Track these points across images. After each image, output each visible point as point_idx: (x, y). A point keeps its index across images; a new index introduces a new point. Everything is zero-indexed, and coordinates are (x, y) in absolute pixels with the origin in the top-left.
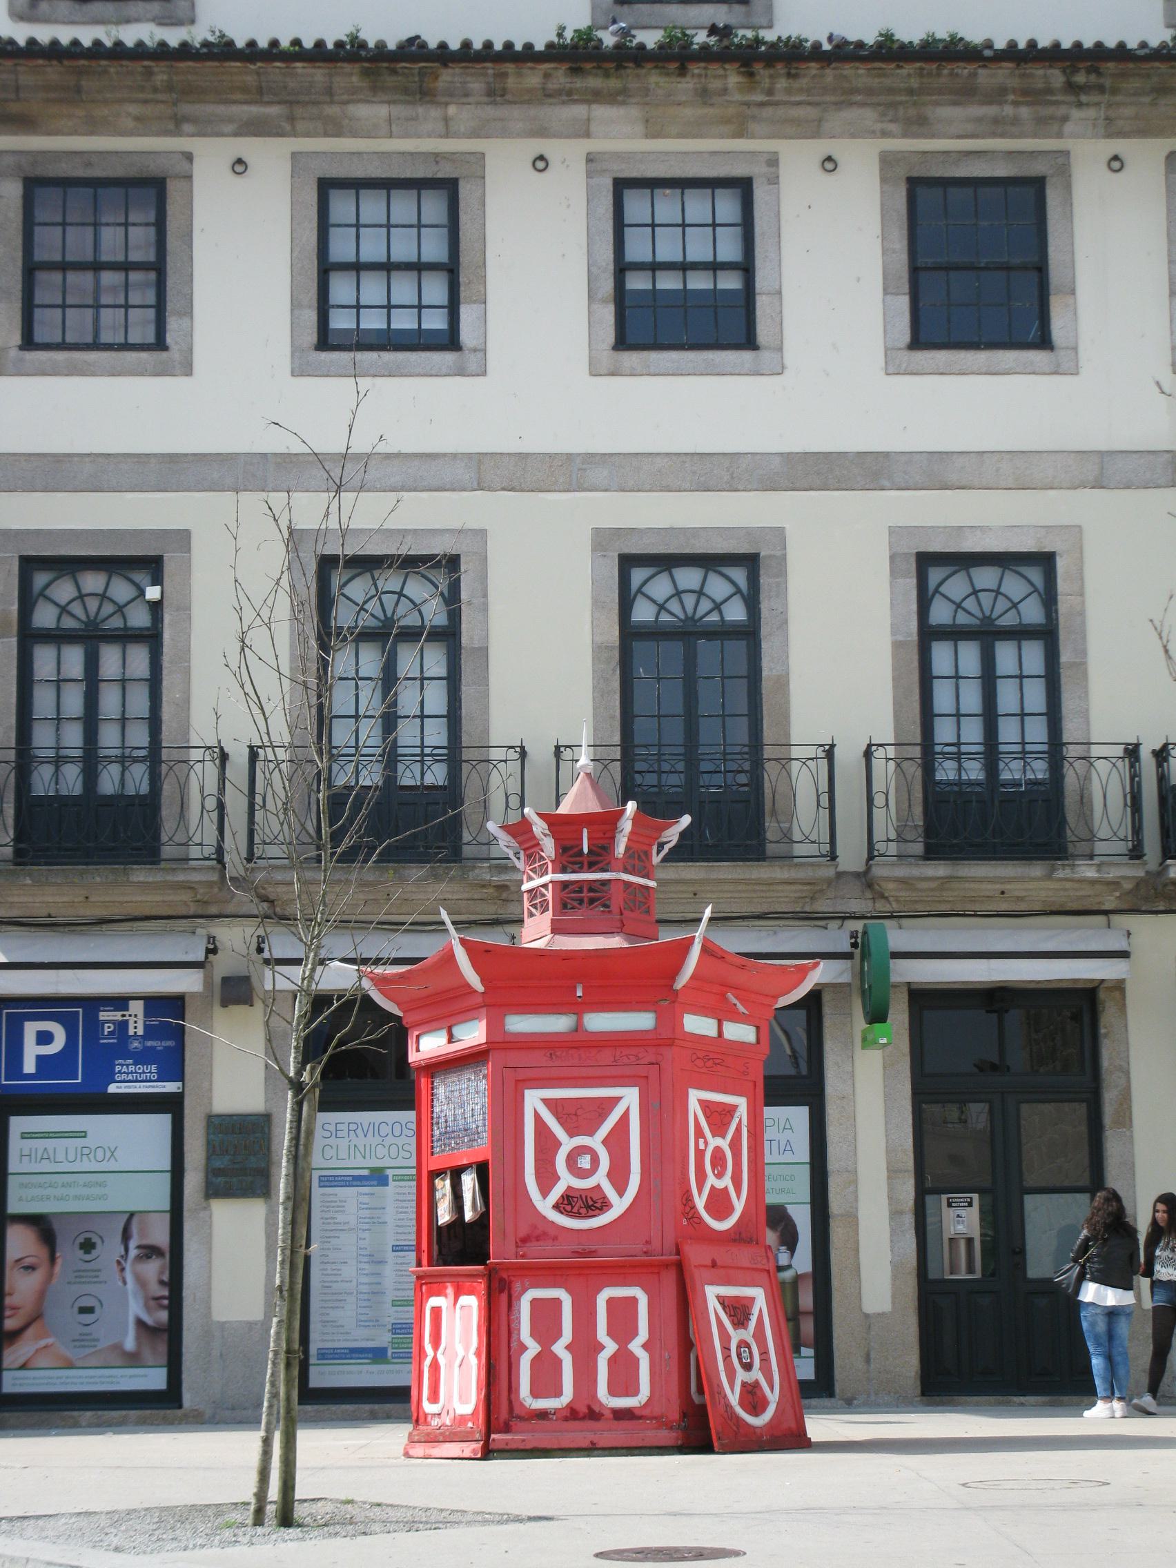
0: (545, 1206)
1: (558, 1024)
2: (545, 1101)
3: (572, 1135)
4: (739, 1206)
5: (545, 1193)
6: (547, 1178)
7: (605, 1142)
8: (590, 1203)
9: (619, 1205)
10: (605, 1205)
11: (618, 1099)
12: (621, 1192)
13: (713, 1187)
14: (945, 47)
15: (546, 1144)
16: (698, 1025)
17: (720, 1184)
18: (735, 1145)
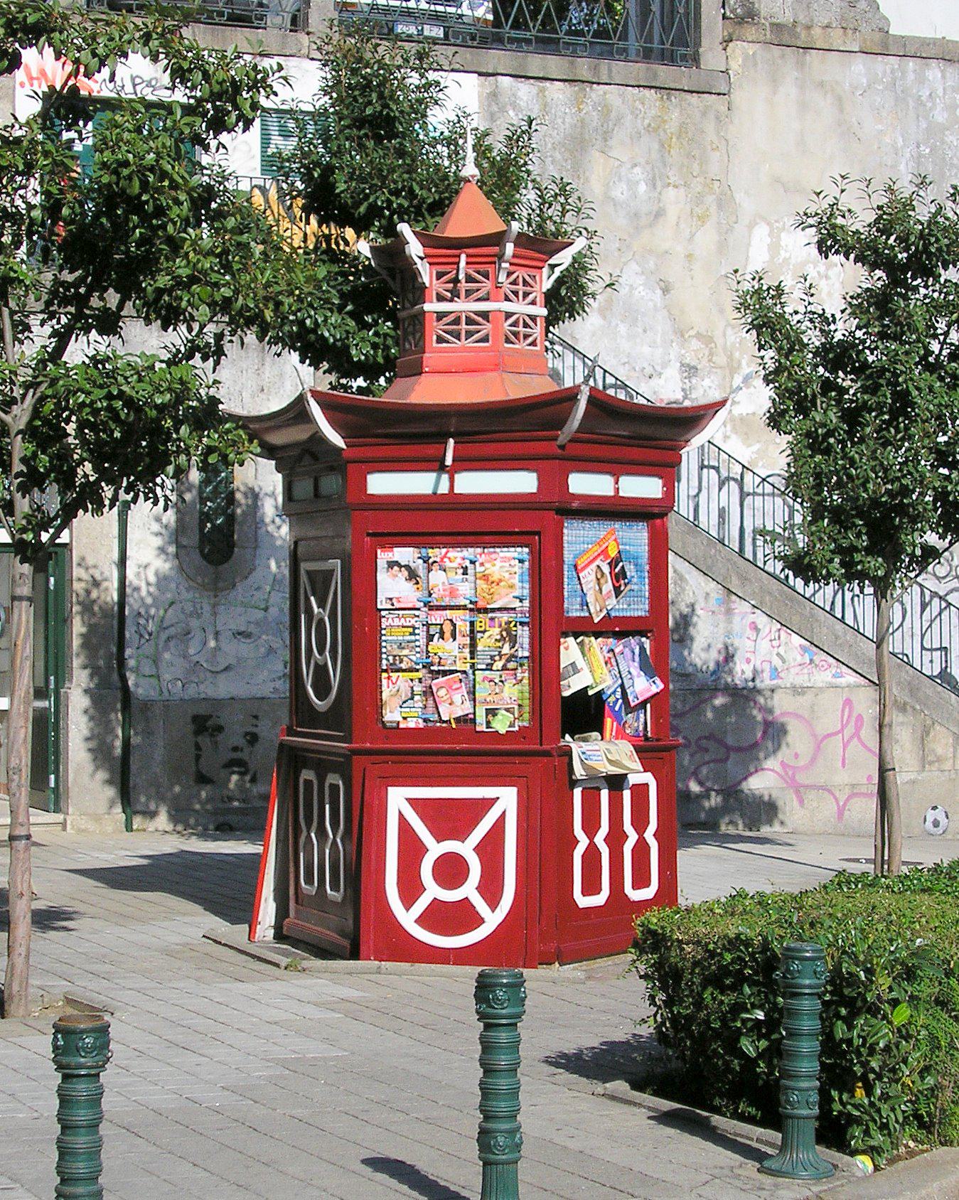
1: (418, 483)
2: (413, 802)
3: (439, 838)
5: (408, 902)
7: (477, 849)
9: (492, 919)
11: (491, 802)
12: (493, 903)
14: (758, 759)
15: (412, 850)
16: (584, 484)
18: (490, 849)
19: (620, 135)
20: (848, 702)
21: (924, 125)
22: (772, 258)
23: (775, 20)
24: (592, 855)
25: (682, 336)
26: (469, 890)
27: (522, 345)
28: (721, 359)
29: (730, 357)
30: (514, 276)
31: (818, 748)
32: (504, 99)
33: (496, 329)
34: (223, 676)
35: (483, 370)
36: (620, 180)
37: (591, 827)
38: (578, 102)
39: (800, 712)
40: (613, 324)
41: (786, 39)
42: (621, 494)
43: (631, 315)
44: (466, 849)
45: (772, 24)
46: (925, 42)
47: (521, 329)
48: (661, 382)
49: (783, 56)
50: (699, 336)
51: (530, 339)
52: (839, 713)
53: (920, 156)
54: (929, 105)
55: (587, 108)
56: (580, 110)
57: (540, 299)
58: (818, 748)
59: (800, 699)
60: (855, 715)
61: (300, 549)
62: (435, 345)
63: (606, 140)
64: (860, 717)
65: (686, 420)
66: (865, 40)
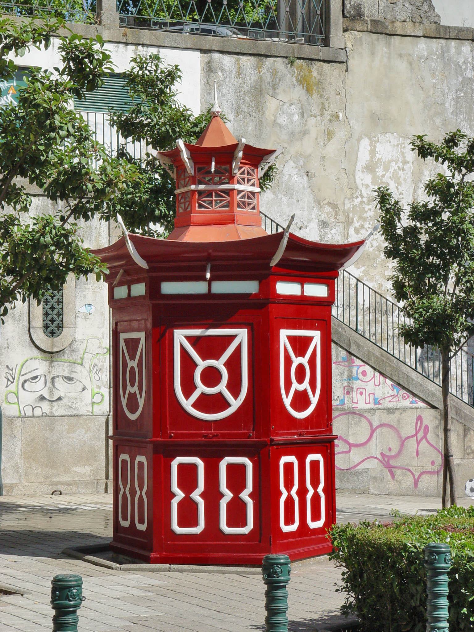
0: (187, 404)
1: (197, 288)
2: (188, 338)
4: (314, 400)
5: (187, 395)
6: (189, 388)
7: (220, 394)
8: (214, 403)
9: (235, 404)
10: (227, 405)
12: (236, 395)
13: (296, 391)
16: (286, 288)
17: (301, 387)
18: (234, 364)
19: (282, 87)
20: (420, 418)
21: (460, 79)
22: (372, 158)
23: (373, 18)
24: (289, 502)
25: (319, 204)
26: (222, 388)
27: (248, 209)
28: (341, 218)
29: (348, 216)
30: (242, 170)
31: (402, 445)
32: (214, 65)
33: (233, 199)
34: (55, 403)
35: (225, 224)
36: (283, 113)
37: (289, 485)
38: (258, 67)
39: (392, 424)
40: (279, 197)
41: (380, 29)
42: (305, 294)
43: (289, 191)
44: (220, 364)
45: (371, 21)
46: (460, 30)
47: (246, 200)
48: (307, 231)
49: (378, 39)
50: (329, 204)
51: (252, 206)
52: (414, 424)
53: (458, 97)
54: (464, 67)
55: (264, 70)
56: (260, 72)
57: (257, 183)
58: (402, 445)
59: (392, 416)
60: (424, 425)
61: (119, 327)
62: (197, 209)
63: (275, 89)
64: (427, 427)
65: (344, 252)
66: (426, 29)
